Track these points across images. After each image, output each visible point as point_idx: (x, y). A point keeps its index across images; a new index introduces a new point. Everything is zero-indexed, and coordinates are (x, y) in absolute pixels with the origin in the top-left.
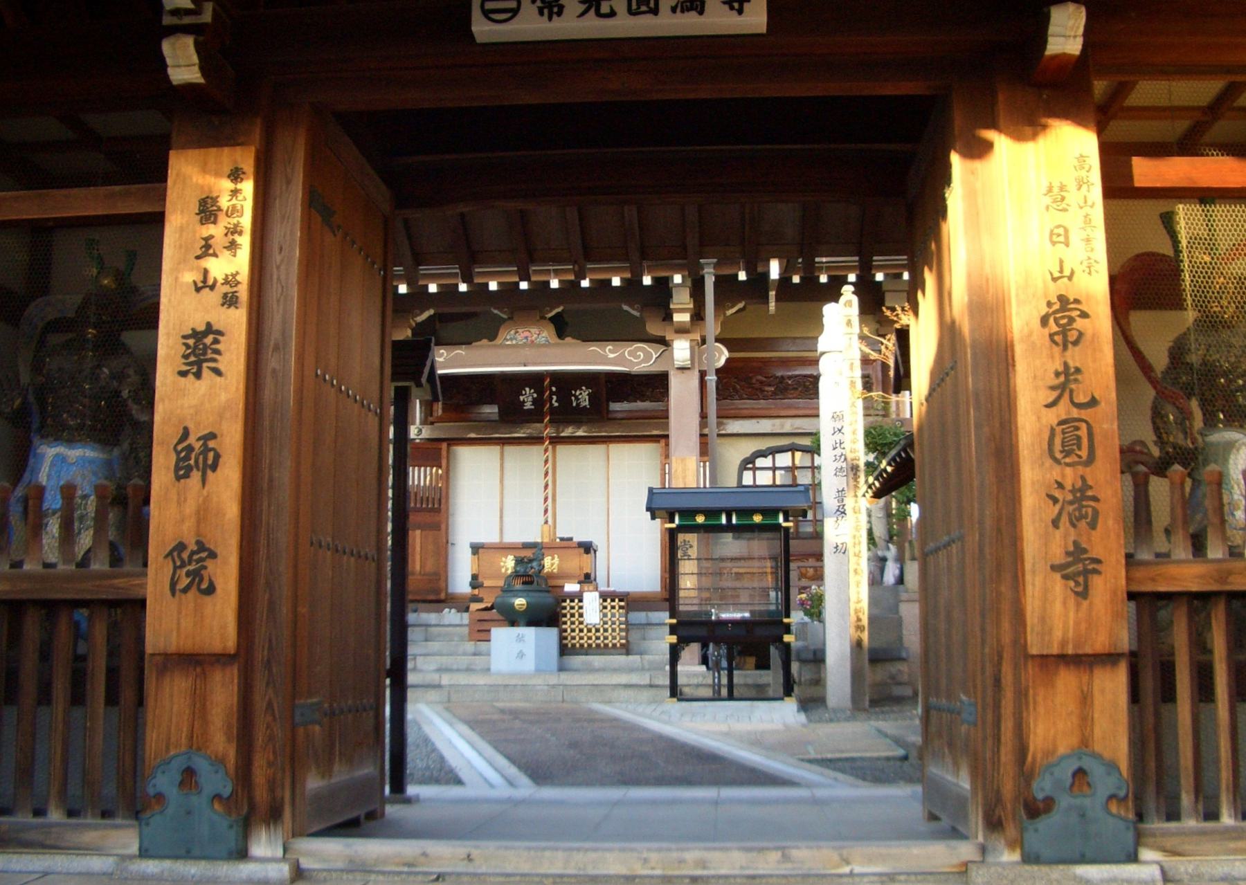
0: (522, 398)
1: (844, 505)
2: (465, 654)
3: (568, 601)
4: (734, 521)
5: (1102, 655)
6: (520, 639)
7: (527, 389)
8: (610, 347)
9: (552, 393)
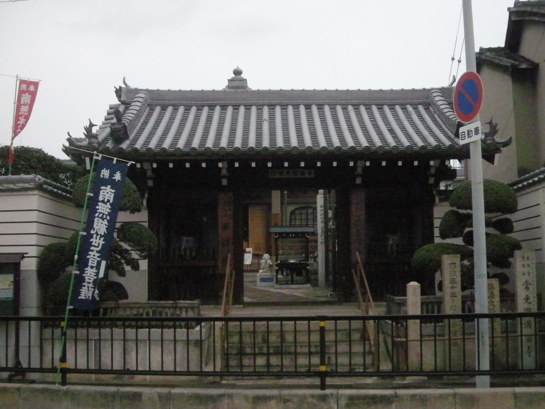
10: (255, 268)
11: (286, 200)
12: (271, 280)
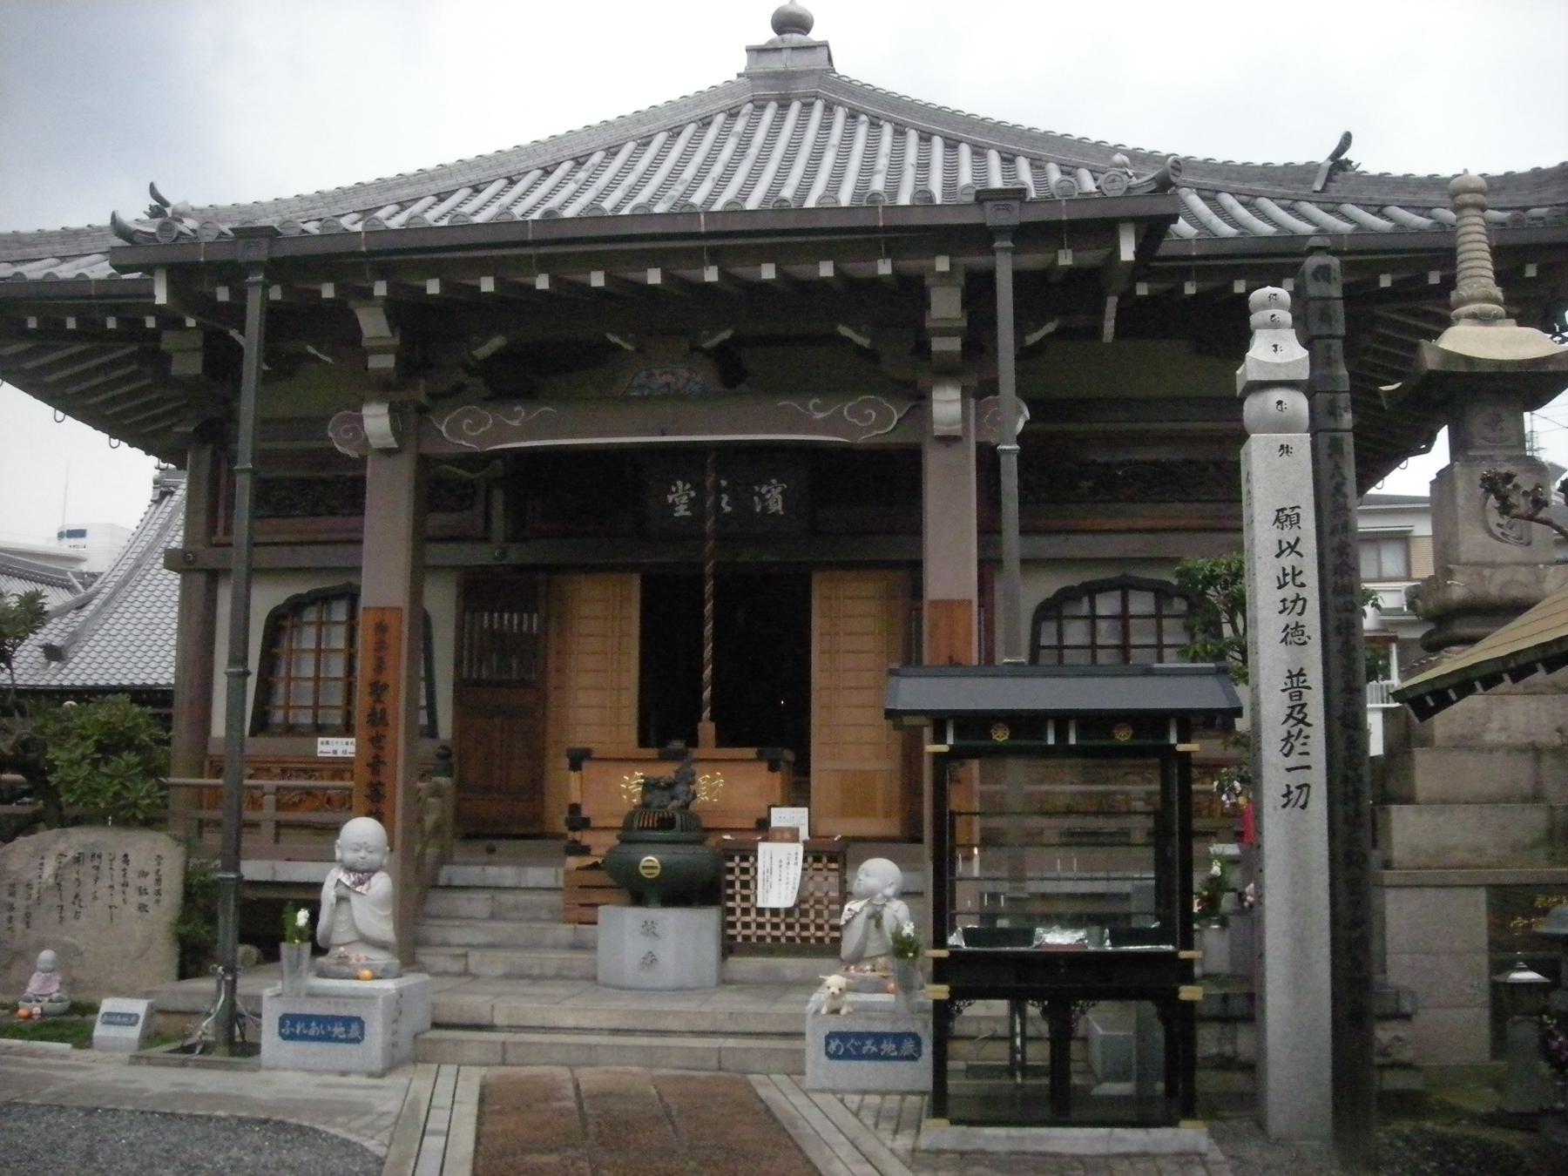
0: (670, 498)
1: (1304, 705)
2: (556, 946)
3: (737, 859)
4: (1072, 741)
7: (680, 483)
8: (818, 401)
9: (719, 490)
10: (819, 928)
11: (1012, 542)
12: (908, 1046)
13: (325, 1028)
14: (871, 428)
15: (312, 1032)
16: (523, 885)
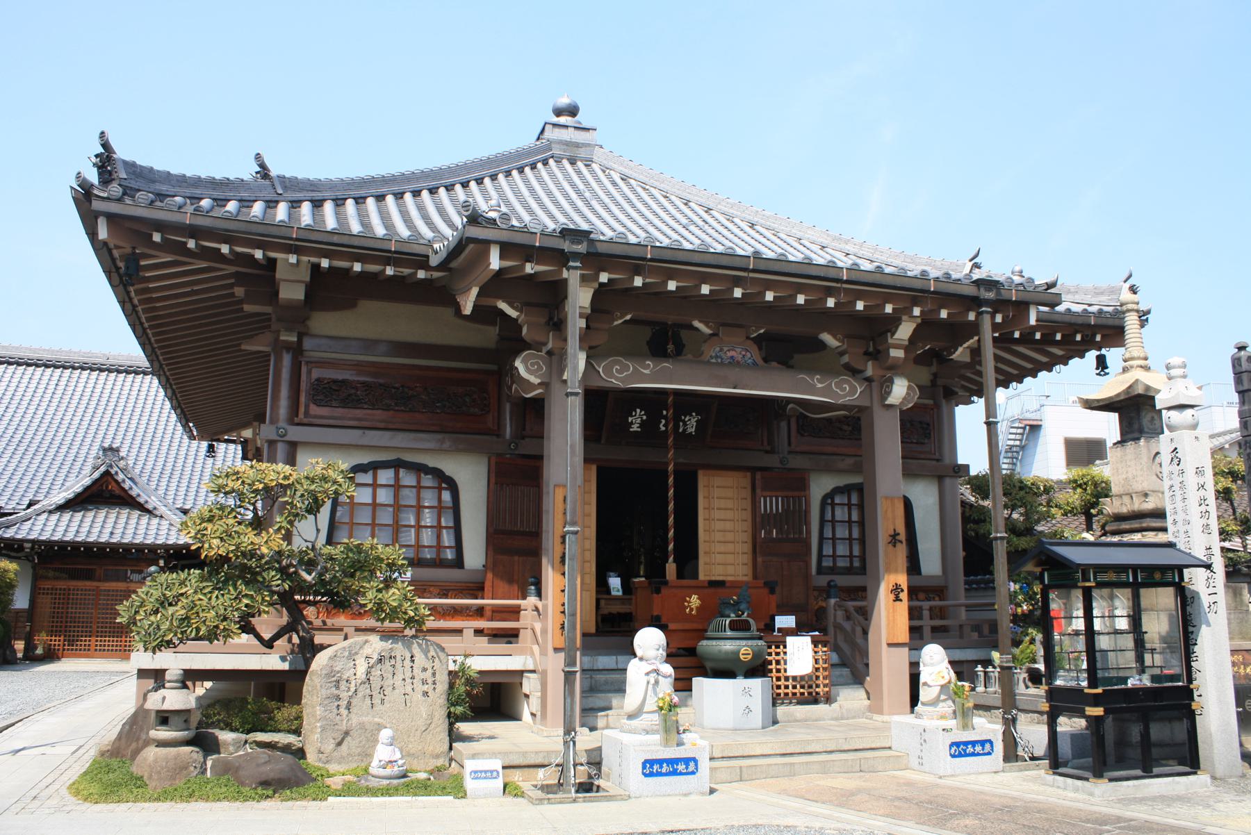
3: (773, 647)
5: (838, 685)
6: (747, 692)
7: (638, 410)
8: (818, 377)
12: (495, 774)
13: (673, 767)
14: (845, 396)
15: (664, 770)
16: (595, 668)
